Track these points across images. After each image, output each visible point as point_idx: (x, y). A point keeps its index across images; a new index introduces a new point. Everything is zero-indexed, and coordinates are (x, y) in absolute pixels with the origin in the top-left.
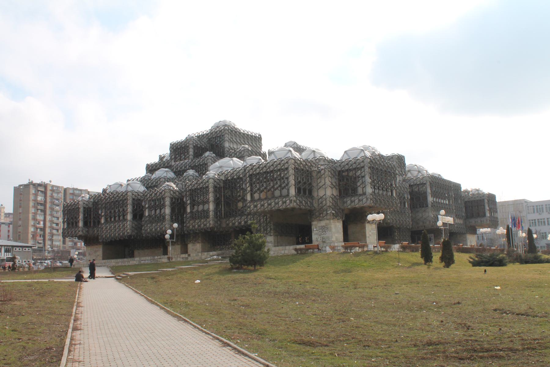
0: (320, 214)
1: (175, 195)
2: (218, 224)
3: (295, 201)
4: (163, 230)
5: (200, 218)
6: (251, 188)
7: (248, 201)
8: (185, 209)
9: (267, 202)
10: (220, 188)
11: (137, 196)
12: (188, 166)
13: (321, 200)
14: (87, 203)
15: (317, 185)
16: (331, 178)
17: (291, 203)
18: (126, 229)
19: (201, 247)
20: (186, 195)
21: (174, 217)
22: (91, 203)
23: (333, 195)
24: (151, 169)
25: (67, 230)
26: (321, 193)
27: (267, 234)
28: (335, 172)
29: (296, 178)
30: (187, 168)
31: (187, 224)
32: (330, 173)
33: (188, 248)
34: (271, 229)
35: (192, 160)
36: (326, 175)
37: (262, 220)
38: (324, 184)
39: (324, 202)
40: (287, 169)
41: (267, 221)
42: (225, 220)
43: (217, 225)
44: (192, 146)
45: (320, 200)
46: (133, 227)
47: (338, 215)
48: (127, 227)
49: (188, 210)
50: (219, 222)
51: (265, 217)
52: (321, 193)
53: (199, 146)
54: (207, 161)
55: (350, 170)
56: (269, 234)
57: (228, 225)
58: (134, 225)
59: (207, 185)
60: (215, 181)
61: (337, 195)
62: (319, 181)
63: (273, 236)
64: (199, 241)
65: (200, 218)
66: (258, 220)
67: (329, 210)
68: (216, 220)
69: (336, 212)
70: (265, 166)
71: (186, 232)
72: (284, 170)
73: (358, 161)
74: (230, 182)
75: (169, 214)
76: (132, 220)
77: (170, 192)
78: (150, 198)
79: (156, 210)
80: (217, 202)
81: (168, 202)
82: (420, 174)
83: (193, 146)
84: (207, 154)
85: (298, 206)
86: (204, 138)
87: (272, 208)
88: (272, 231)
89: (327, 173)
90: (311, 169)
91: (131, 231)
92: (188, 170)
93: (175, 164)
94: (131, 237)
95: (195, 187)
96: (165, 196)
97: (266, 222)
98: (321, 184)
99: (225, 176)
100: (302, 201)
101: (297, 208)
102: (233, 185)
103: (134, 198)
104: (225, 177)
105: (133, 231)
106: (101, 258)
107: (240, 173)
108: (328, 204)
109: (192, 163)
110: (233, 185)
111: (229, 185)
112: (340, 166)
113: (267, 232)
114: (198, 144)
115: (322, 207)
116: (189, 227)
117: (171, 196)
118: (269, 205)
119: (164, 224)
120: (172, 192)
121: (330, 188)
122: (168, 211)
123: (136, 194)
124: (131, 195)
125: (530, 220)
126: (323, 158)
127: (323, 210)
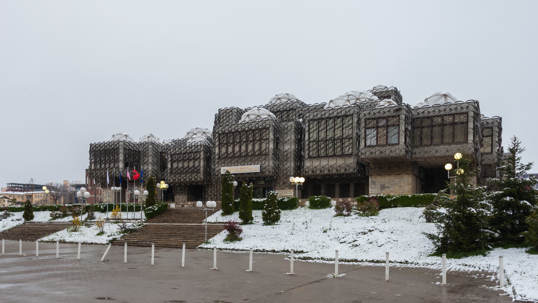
4: (192, 180)
6: (171, 159)
7: (169, 168)
26: (287, 147)
39: (147, 174)
45: (285, 171)
49: (169, 166)
56: (184, 193)
61: (158, 169)
79: (110, 164)
98: (145, 161)
123: (128, 144)
124: (123, 145)
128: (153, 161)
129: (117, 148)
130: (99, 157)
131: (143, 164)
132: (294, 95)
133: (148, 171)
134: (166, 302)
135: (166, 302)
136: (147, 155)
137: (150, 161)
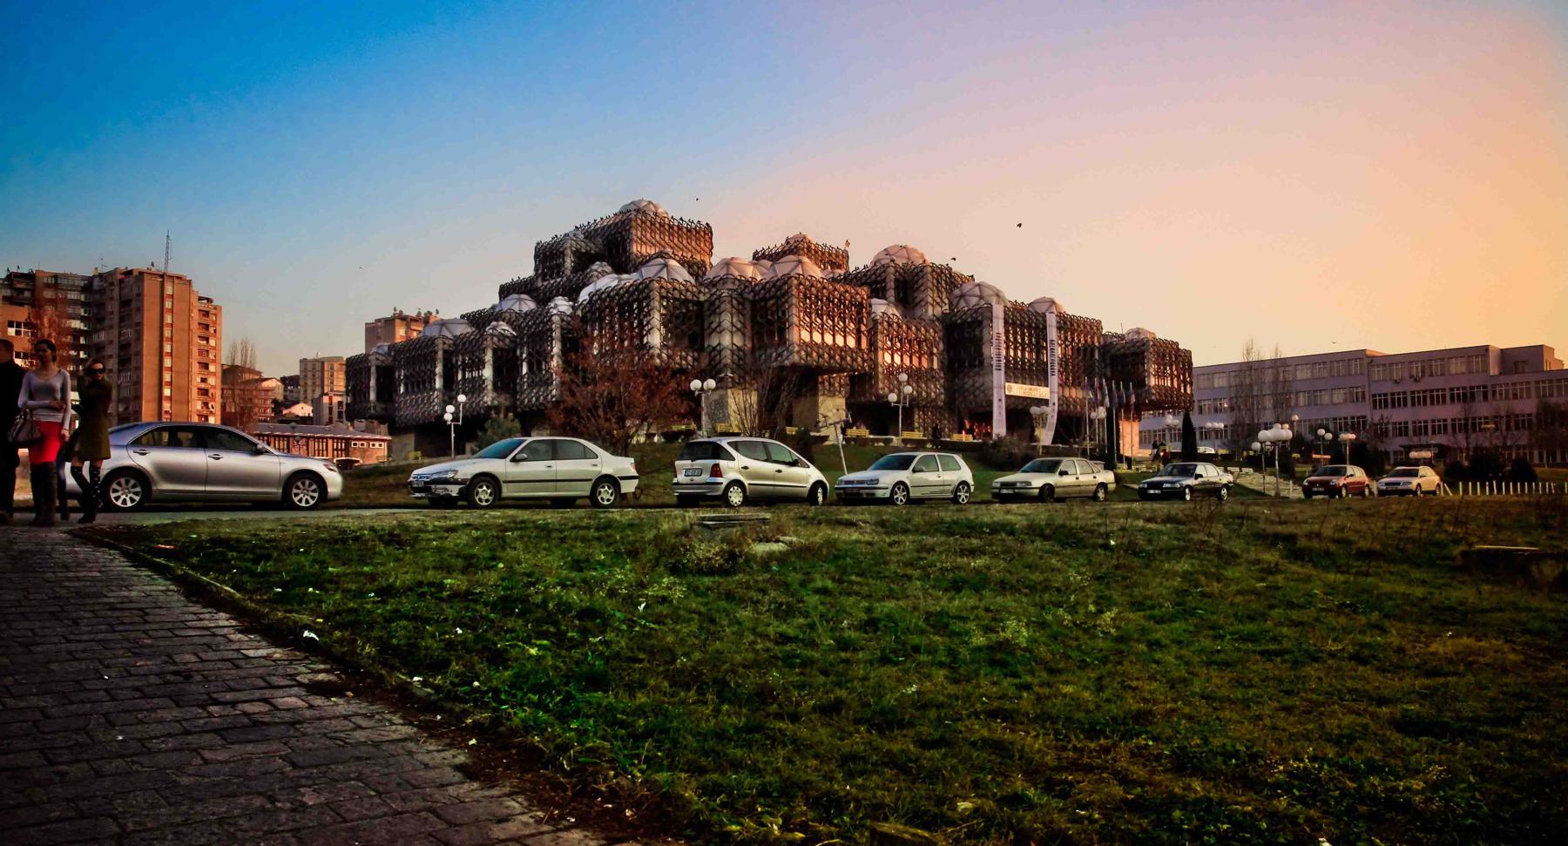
40: (884, 280)
70: (865, 275)
72: (880, 282)
82: (982, 302)
98: (714, 326)
116: (523, 402)
120: (495, 339)
122: (488, 373)
125: (1374, 396)
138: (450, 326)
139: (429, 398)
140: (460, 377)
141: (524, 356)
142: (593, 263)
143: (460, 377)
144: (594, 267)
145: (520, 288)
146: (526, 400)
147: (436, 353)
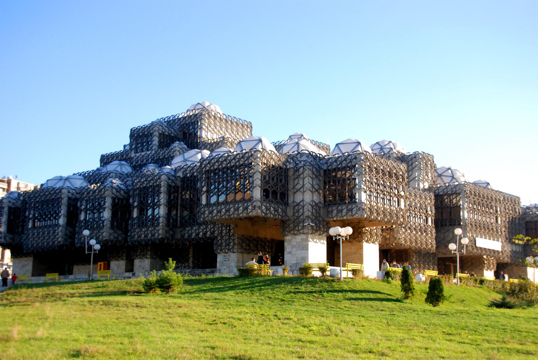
0: (295, 227)
1: (118, 194)
2: (170, 234)
3: (260, 208)
5: (141, 226)
8: (131, 212)
9: (225, 208)
10: (176, 188)
11: (75, 194)
12: (150, 160)
13: (296, 208)
14: (15, 201)
15: (293, 188)
16: (312, 179)
17: (255, 209)
18: (57, 237)
19: (149, 263)
20: (133, 194)
21: (115, 224)
22: (20, 202)
23: (313, 201)
24: (106, 160)
25: (32, 231)
26: (298, 198)
27: (229, 250)
28: (318, 171)
29: (263, 177)
30: (149, 161)
31: (132, 233)
32: (311, 172)
33: (135, 264)
34: (234, 244)
35: (156, 152)
36: (305, 175)
37: (224, 231)
38: (303, 187)
39: (301, 211)
41: (231, 233)
42: (180, 230)
43: (168, 235)
44: (157, 133)
46: (66, 235)
47: (320, 228)
48: (58, 234)
49: (135, 214)
50: (171, 233)
51: (228, 228)
52: (298, 198)
53: (167, 133)
54: (173, 153)
55: (339, 170)
57: (183, 236)
58: (68, 232)
59: (158, 183)
60: (169, 179)
61: (320, 202)
62: (296, 182)
63: (236, 254)
64: (148, 256)
65: (141, 226)
66: (220, 232)
67: (306, 221)
68: (167, 229)
69: (316, 224)
71: (130, 244)
73: (349, 158)
74: (188, 181)
75: (110, 219)
76: (65, 225)
77: (112, 190)
78: (99, 196)
80: (171, 205)
81: (108, 203)
83: (159, 133)
84: (177, 144)
85: (263, 215)
86: (175, 124)
87: (221, 216)
88: (236, 247)
89: (306, 172)
90: (286, 166)
91: (63, 239)
92: (150, 163)
93: (135, 156)
94: (108, 242)
95: (144, 185)
96: (105, 195)
97: (229, 234)
98: (298, 187)
99: (183, 172)
100: (270, 208)
101: (262, 217)
102: (193, 184)
103: (71, 196)
104: (183, 174)
105: (66, 240)
106: (30, 274)
107: (188, 172)
108: (306, 214)
109: (155, 156)
110: (193, 184)
111: (187, 184)
112: (326, 163)
113: (229, 247)
114: (165, 132)
115: (298, 217)
116: (133, 237)
117: (113, 196)
118: (219, 212)
119: (101, 231)
120: (114, 191)
121: (310, 192)
122: (107, 214)
123: (74, 191)
126: (307, 152)
127: (299, 221)
128: (312, 185)
129: (158, 185)
130: (151, 197)
131: (294, 193)
132: (59, 175)
133: (304, 206)
134: (443, 358)
135: (443, 358)
136: (302, 176)
137: (308, 186)
138: (70, 180)
139: (54, 232)
140: (30, 225)
141: (136, 204)
142: (173, 142)
143: (30, 225)
144: (174, 145)
145: (122, 156)
146: (51, 243)
147: (3, 208)
